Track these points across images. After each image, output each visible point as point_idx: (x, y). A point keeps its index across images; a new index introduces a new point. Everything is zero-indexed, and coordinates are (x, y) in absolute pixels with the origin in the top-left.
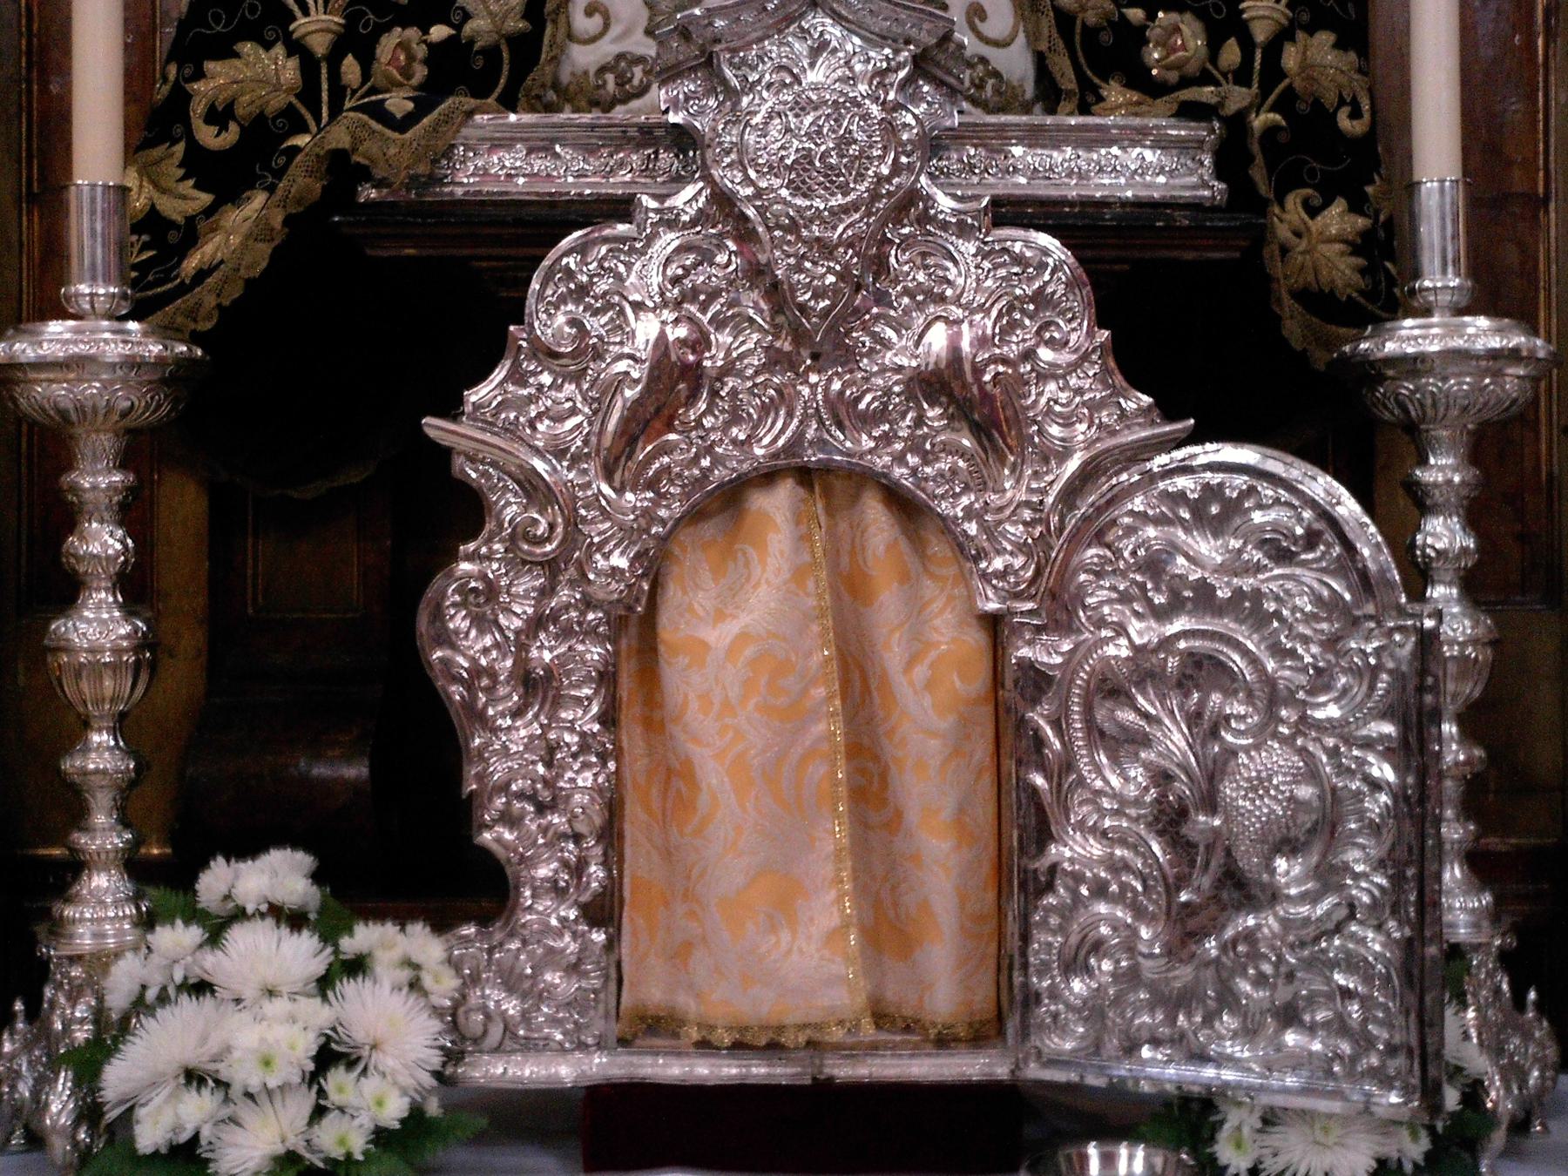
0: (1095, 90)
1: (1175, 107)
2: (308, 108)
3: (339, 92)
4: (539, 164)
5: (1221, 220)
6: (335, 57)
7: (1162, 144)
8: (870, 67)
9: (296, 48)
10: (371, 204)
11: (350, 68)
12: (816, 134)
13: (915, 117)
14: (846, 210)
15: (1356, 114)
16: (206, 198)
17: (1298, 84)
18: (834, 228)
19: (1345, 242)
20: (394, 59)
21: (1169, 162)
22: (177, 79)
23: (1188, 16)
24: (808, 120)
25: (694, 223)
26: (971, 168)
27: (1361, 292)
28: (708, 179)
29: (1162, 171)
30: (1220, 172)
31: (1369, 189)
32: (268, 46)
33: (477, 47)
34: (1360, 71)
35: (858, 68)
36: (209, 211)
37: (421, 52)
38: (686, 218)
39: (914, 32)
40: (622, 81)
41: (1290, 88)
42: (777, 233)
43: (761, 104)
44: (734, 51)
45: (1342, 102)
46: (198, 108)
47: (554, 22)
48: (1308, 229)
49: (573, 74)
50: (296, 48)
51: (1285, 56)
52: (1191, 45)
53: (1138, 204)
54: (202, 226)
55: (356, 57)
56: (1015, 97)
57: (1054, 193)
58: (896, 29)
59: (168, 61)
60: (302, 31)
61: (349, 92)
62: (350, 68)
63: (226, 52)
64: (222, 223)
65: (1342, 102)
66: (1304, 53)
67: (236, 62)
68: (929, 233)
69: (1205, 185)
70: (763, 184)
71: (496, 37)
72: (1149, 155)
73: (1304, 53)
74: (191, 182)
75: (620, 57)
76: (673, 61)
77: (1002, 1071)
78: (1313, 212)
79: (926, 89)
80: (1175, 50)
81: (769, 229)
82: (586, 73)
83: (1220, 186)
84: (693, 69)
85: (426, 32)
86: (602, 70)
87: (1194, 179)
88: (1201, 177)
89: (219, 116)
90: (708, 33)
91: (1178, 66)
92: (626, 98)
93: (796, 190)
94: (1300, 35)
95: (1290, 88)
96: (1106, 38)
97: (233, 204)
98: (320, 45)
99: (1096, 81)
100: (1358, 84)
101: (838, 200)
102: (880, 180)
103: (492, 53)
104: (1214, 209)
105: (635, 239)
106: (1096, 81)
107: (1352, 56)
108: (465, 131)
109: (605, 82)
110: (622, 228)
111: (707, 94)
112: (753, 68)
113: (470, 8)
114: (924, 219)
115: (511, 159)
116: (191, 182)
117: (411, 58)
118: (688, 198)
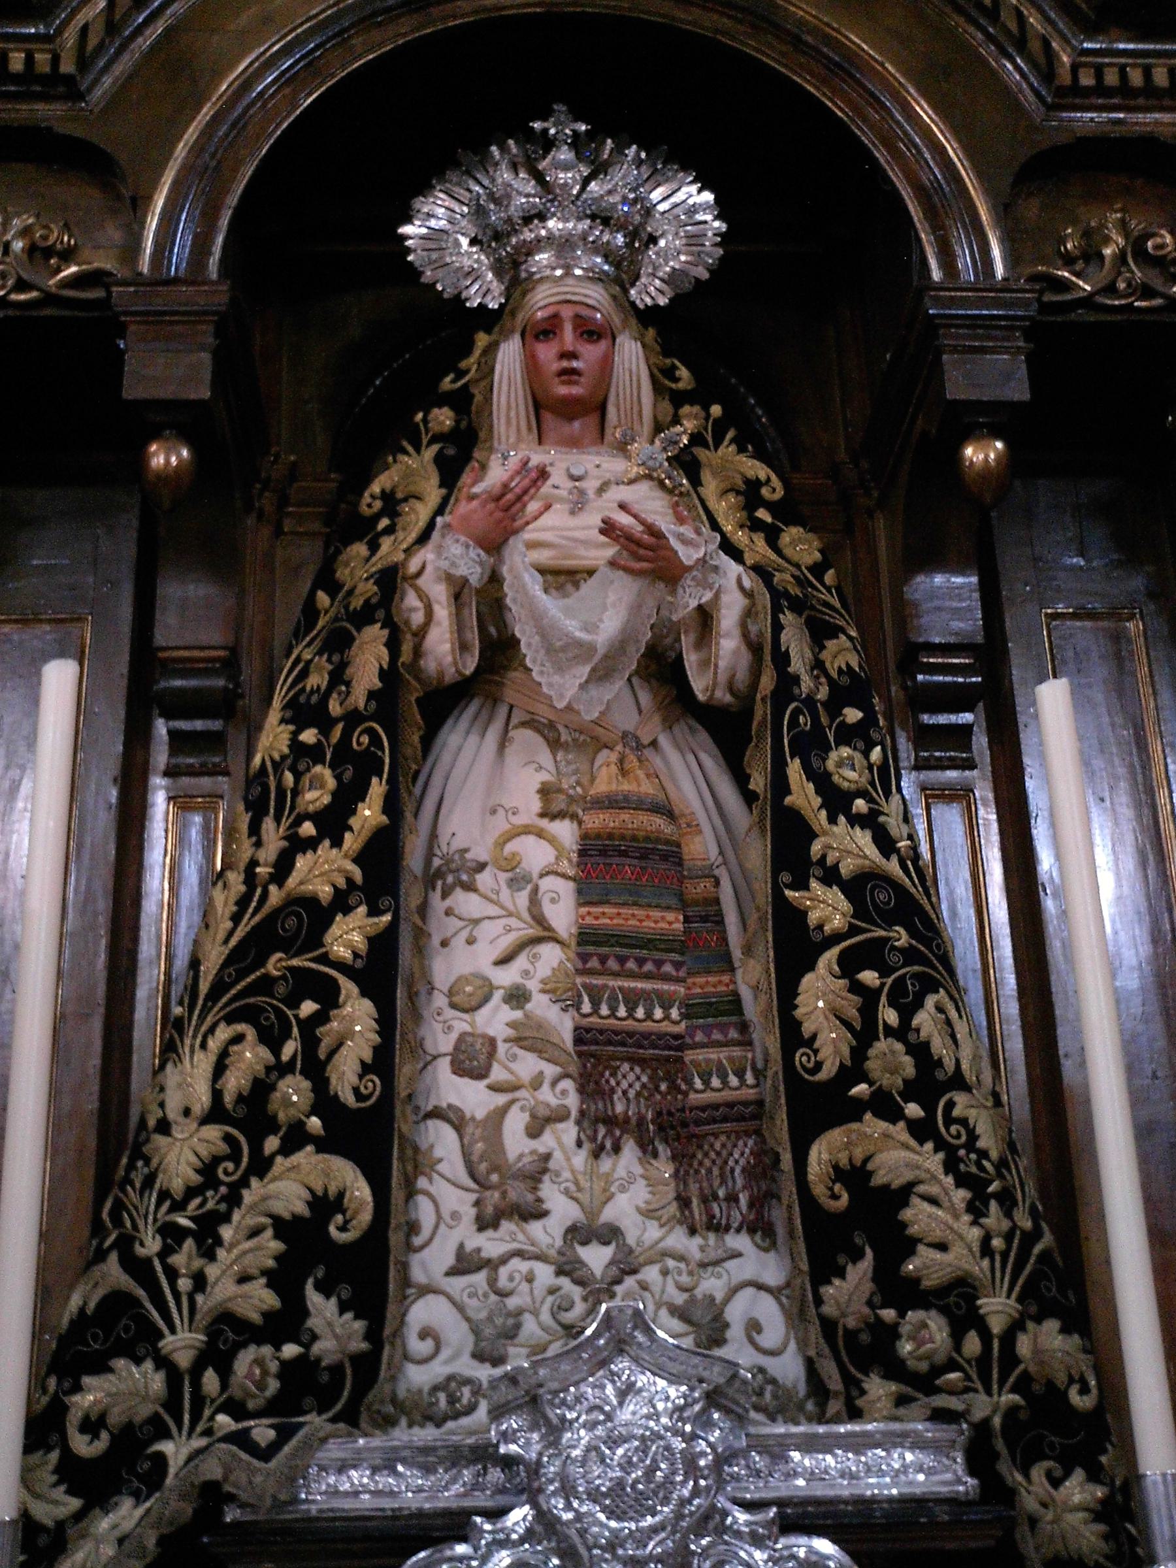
0: (857, 1383)
1: (929, 1413)
2: (172, 1416)
3: (199, 1401)
4: (386, 1481)
5: (976, 1513)
6: (197, 1371)
7: (918, 1444)
8: (670, 1405)
9: (164, 1363)
10: (236, 1524)
11: (210, 1380)
12: (627, 1465)
13: (709, 1444)
14: (655, 1529)
15: (1084, 1390)
16: (75, 1503)
17: (1032, 1369)
18: (645, 1546)
19: (1087, 1509)
20: (249, 1375)
21: (928, 1460)
22: (56, 1392)
23: (933, 1313)
24: (620, 1451)
25: (522, 1540)
26: (758, 1474)
27: (1107, 1557)
28: (535, 1505)
29: (921, 1470)
30: (972, 1471)
31: (1103, 1459)
32: (138, 1361)
33: (323, 1364)
34: (1085, 1351)
35: (660, 1406)
36: (79, 1516)
37: (274, 1366)
38: (514, 1536)
39: (706, 1374)
40: (452, 1400)
41: (1025, 1372)
42: (596, 1552)
43: (579, 1439)
44: (555, 1393)
45: (1071, 1380)
46: (74, 1419)
47: (392, 1344)
48: (1053, 1500)
49: (408, 1391)
50: (164, 1363)
51: (1019, 1344)
52: (938, 1337)
53: (903, 1500)
54: (71, 1532)
55: (216, 1371)
56: (790, 1398)
57: (831, 1493)
58: (691, 1371)
59: (48, 1375)
60: (170, 1347)
61: (208, 1401)
62: (210, 1380)
63: (101, 1367)
64: (92, 1530)
65: (1071, 1380)
66: (1035, 1341)
67: (111, 1377)
68: (726, 1543)
69: (959, 1481)
70: (584, 1509)
71: (340, 1356)
72: (909, 1457)
73: (1035, 1341)
74: (62, 1488)
75: (450, 1378)
76: (503, 1400)
77: (230, 212)
78: (1056, 1483)
79: (716, 1416)
80: (923, 1343)
81: (589, 1549)
82: (420, 1391)
83: (970, 1481)
84: (519, 1407)
85: (278, 1348)
86: (435, 1389)
87: (948, 1476)
88: (955, 1472)
89: (92, 1425)
90: (533, 1381)
91: (928, 1357)
92: (457, 1416)
93: (611, 1514)
94: (1030, 1325)
95: (1025, 1372)
96: (865, 1338)
97: (102, 1508)
98: (184, 1360)
99: (859, 1376)
100: (1084, 1364)
101: (649, 1520)
102: (683, 1502)
103: (337, 1370)
104: (969, 1503)
105: (471, 1558)
106: (859, 1376)
107: (1076, 1338)
108: (319, 1455)
109: (438, 1401)
110: (461, 1549)
111: (531, 1429)
112: (571, 1409)
113: (317, 1331)
114: (722, 1530)
115: (358, 1477)
116: (62, 1488)
117: (265, 1373)
118: (519, 1517)
